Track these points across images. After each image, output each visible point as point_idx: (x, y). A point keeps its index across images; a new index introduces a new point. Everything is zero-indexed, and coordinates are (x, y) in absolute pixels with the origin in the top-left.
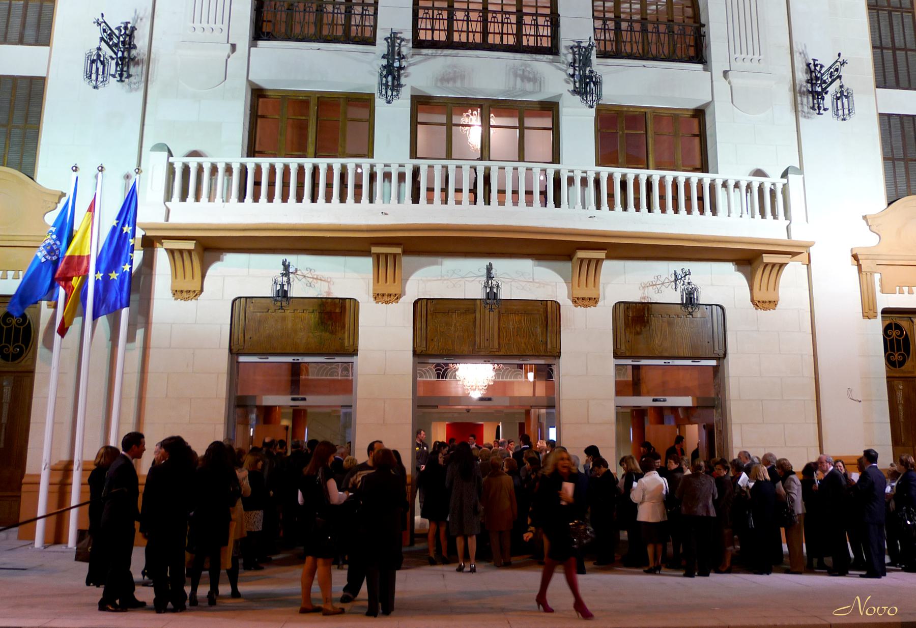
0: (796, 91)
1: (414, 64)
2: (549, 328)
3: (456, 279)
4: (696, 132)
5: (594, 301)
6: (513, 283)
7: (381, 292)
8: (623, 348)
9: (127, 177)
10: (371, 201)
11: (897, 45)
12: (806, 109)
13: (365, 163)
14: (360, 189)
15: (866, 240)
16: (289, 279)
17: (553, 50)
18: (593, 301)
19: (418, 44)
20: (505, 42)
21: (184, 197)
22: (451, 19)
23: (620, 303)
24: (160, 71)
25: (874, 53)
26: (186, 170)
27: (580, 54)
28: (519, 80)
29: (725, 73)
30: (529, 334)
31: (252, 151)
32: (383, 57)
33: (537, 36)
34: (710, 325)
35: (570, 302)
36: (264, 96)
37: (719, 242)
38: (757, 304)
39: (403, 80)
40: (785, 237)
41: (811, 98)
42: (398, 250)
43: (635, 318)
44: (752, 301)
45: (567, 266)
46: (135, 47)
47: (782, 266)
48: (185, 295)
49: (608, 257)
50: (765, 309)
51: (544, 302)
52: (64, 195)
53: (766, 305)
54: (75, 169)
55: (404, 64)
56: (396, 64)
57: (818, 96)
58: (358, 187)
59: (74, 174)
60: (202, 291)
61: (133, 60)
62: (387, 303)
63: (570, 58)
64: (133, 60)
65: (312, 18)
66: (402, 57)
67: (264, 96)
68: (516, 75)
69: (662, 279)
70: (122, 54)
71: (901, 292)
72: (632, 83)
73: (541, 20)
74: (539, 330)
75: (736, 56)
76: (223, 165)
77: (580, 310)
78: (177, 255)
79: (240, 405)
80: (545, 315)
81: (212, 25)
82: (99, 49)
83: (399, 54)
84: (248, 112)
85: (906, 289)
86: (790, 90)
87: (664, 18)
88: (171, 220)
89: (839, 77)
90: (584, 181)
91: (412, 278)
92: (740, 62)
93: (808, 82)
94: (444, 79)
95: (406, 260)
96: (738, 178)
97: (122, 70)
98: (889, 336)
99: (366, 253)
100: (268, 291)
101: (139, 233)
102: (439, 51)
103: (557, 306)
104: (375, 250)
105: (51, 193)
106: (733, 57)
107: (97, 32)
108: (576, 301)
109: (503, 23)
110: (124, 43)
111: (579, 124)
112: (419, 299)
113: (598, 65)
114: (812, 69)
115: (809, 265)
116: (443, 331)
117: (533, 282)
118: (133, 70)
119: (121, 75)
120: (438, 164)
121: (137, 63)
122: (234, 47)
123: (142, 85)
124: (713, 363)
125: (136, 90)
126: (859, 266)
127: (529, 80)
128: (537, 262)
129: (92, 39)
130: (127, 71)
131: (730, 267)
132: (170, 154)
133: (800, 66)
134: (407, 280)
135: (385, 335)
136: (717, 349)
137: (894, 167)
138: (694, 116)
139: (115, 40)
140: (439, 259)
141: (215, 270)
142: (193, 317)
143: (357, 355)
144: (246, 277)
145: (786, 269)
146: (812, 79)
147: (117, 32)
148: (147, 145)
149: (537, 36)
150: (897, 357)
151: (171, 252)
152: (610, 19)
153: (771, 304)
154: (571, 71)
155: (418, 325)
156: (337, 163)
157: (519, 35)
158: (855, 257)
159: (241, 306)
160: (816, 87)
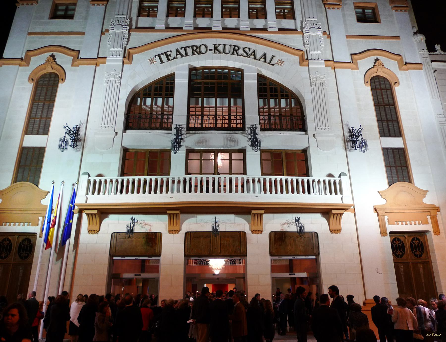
0: (345, 141)
1: (187, 137)
2: (242, 243)
3: (202, 223)
4: (127, 161)
5: (261, 231)
6: (226, 225)
7: (171, 229)
8: (274, 252)
9: (73, 185)
10: (254, 192)
11: (389, 119)
12: (350, 148)
13: (165, 178)
14: (164, 187)
15: (381, 202)
16: (134, 225)
17: (243, 129)
18: (260, 231)
19: (189, 129)
20: (196, 126)
21: (93, 193)
22: (202, 119)
23: (272, 232)
24: (88, 143)
25: (378, 123)
26: (95, 182)
27: (253, 130)
28: (228, 141)
29: (314, 135)
30: (233, 246)
31: (123, 173)
32: (175, 135)
33: (209, 123)
34: (312, 241)
35: (250, 232)
36: (128, 151)
37: (116, 205)
38: (332, 231)
39: (182, 144)
40: (341, 202)
41: (351, 143)
42: (178, 212)
43: (278, 240)
44: (330, 230)
45: (249, 216)
46: (79, 135)
47: (341, 214)
48: (93, 232)
49: (265, 213)
50: (336, 233)
51: (239, 233)
52: (49, 192)
53: (336, 232)
54: (53, 183)
55: (183, 137)
56: (180, 138)
57: (354, 142)
58: (242, 186)
59: (53, 185)
60: (99, 230)
61: (79, 140)
62: (174, 234)
63: (249, 132)
64: (79, 140)
65: (148, 120)
66: (182, 135)
67: (128, 151)
68: (227, 139)
69: (290, 221)
70: (75, 137)
71: (398, 224)
72: (276, 141)
73: (238, 117)
74: (237, 244)
75: (319, 127)
76: (115, 180)
77: (255, 235)
78: (90, 216)
79: (114, 277)
80: (239, 238)
81: (109, 125)
82: (65, 137)
83: (181, 133)
84: (122, 158)
85: (400, 223)
86: (342, 140)
87: (288, 114)
88: (88, 202)
89: (361, 135)
90: (179, 182)
91: (184, 223)
92: (320, 130)
93: (350, 136)
94: (199, 142)
95: (182, 216)
96: (319, 178)
97: (74, 144)
98: (395, 244)
99: (164, 213)
100: (124, 229)
101: (76, 207)
102: (197, 132)
103: (245, 234)
104: (168, 212)
105: (44, 192)
106: (317, 128)
107: (65, 130)
108: (253, 232)
109: (223, 119)
110: (75, 133)
111: (254, 159)
112: (187, 232)
113: (260, 135)
114: (351, 131)
115: (355, 213)
116: (199, 246)
117: (235, 224)
118: (78, 143)
119: (73, 146)
120: (240, 177)
121: (80, 141)
122: (116, 133)
123: (81, 149)
124: (314, 257)
125: (79, 151)
126: (378, 213)
127: (233, 141)
128: (236, 216)
129: (62, 133)
130: (76, 144)
131: (319, 215)
132: (89, 176)
133: (346, 130)
134: (182, 224)
135: (173, 247)
136: (315, 251)
137: (391, 170)
138: (302, 152)
139: (72, 133)
140: (196, 215)
141: (105, 222)
142: (96, 241)
143: (161, 256)
144: (116, 224)
145: (343, 216)
146: (351, 135)
147: (73, 130)
148: (82, 172)
149: (209, 123)
150: (399, 253)
151: (88, 215)
152: (266, 116)
153: (338, 231)
154: (250, 137)
155: (187, 243)
156: (153, 178)
157: (229, 123)
158: (375, 209)
159: (115, 236)
160: (353, 139)
